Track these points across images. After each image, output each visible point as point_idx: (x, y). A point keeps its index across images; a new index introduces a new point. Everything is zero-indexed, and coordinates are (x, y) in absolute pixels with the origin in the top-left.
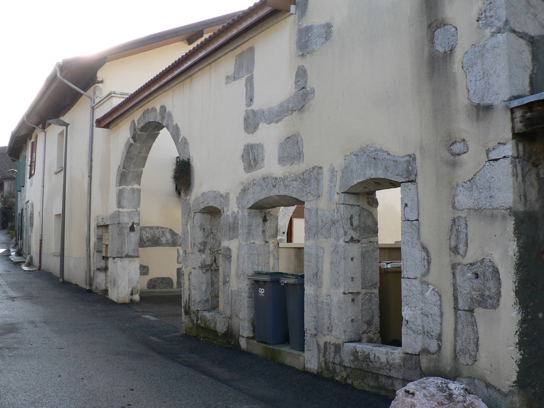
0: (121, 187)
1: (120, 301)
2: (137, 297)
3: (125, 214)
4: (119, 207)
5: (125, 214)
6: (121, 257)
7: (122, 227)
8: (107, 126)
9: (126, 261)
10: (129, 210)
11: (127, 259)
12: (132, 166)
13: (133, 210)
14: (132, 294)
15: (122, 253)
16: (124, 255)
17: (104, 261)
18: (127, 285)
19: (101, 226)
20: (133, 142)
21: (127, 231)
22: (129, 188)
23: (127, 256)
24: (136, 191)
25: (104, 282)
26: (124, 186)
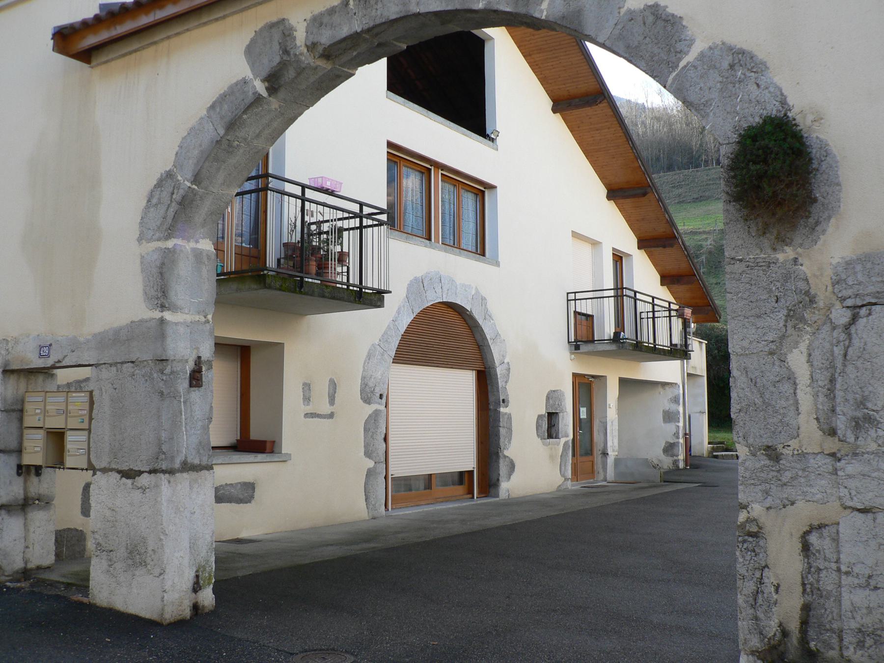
0: (170, 244)
1: (170, 615)
2: (207, 597)
3: (181, 329)
4: (163, 307)
5: (181, 329)
6: (171, 472)
7: (172, 372)
8: (86, 56)
9: (184, 478)
10: (188, 318)
11: (185, 475)
12: (221, 177)
13: (197, 318)
14: (197, 587)
15: (172, 458)
16: (177, 465)
17: (20, 480)
18: (186, 561)
19: (13, 372)
20: (264, 93)
21: (183, 384)
22: (189, 246)
23: (187, 467)
24: (205, 260)
25: (20, 546)
26: (179, 242)
